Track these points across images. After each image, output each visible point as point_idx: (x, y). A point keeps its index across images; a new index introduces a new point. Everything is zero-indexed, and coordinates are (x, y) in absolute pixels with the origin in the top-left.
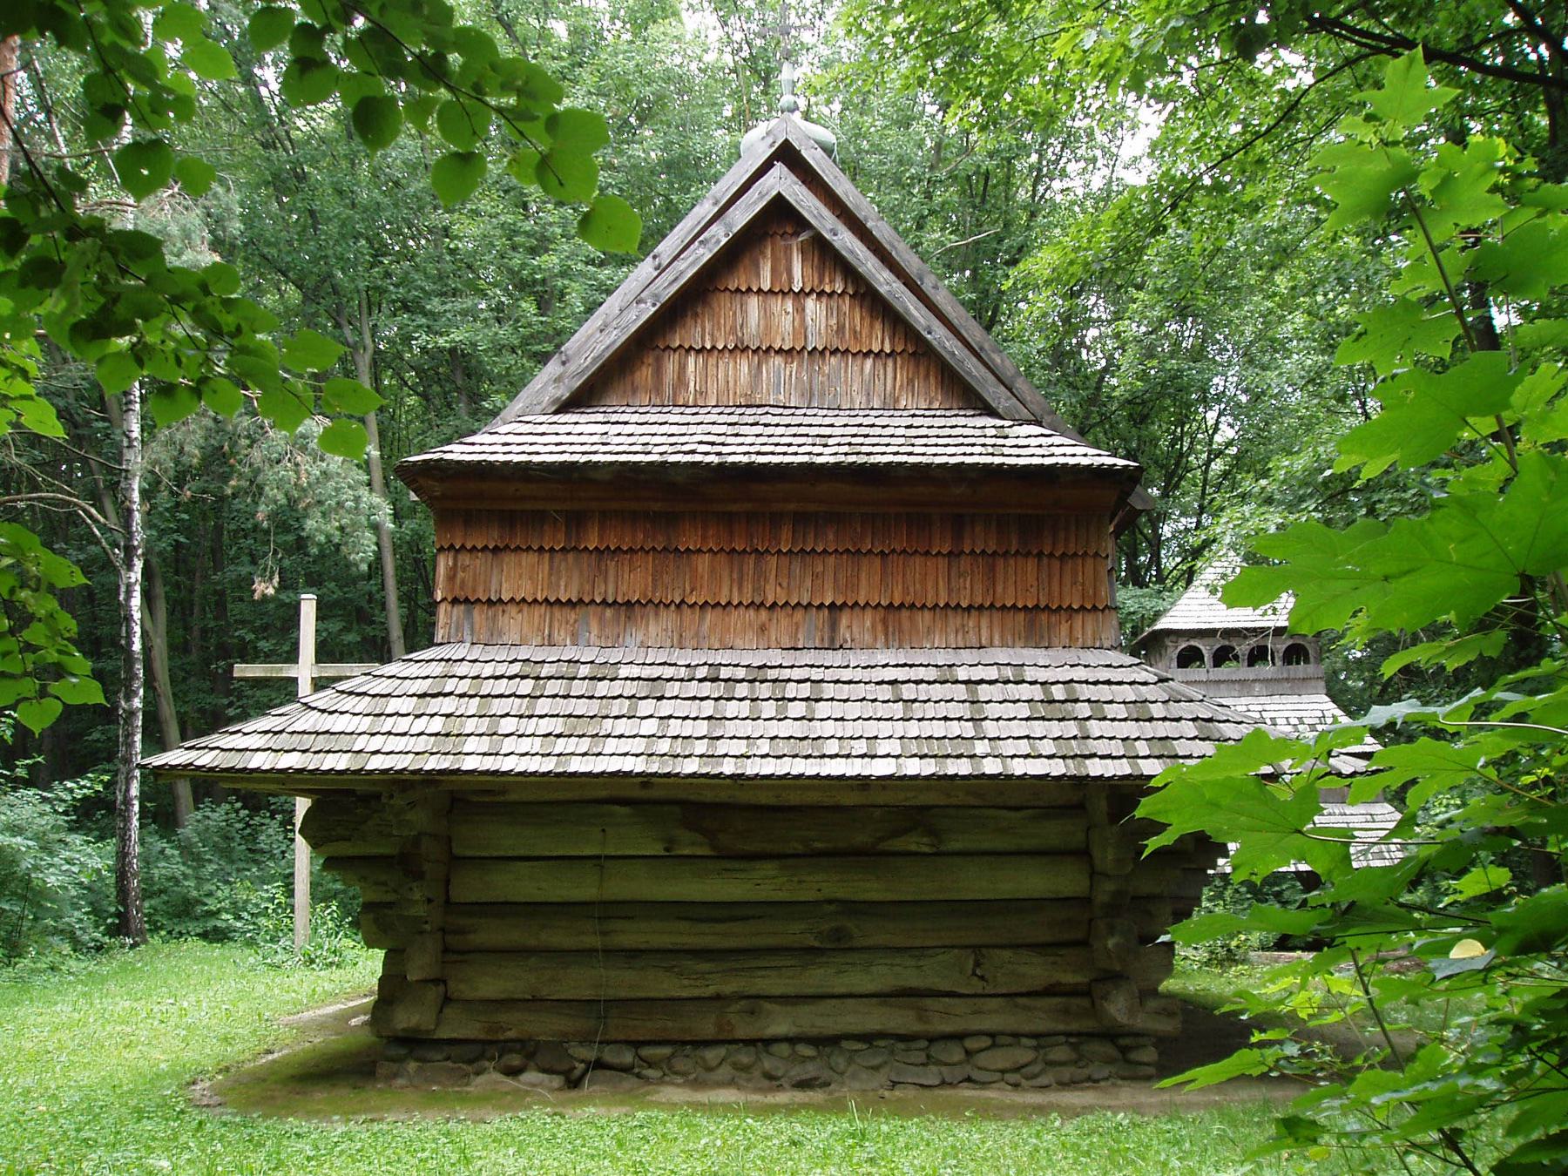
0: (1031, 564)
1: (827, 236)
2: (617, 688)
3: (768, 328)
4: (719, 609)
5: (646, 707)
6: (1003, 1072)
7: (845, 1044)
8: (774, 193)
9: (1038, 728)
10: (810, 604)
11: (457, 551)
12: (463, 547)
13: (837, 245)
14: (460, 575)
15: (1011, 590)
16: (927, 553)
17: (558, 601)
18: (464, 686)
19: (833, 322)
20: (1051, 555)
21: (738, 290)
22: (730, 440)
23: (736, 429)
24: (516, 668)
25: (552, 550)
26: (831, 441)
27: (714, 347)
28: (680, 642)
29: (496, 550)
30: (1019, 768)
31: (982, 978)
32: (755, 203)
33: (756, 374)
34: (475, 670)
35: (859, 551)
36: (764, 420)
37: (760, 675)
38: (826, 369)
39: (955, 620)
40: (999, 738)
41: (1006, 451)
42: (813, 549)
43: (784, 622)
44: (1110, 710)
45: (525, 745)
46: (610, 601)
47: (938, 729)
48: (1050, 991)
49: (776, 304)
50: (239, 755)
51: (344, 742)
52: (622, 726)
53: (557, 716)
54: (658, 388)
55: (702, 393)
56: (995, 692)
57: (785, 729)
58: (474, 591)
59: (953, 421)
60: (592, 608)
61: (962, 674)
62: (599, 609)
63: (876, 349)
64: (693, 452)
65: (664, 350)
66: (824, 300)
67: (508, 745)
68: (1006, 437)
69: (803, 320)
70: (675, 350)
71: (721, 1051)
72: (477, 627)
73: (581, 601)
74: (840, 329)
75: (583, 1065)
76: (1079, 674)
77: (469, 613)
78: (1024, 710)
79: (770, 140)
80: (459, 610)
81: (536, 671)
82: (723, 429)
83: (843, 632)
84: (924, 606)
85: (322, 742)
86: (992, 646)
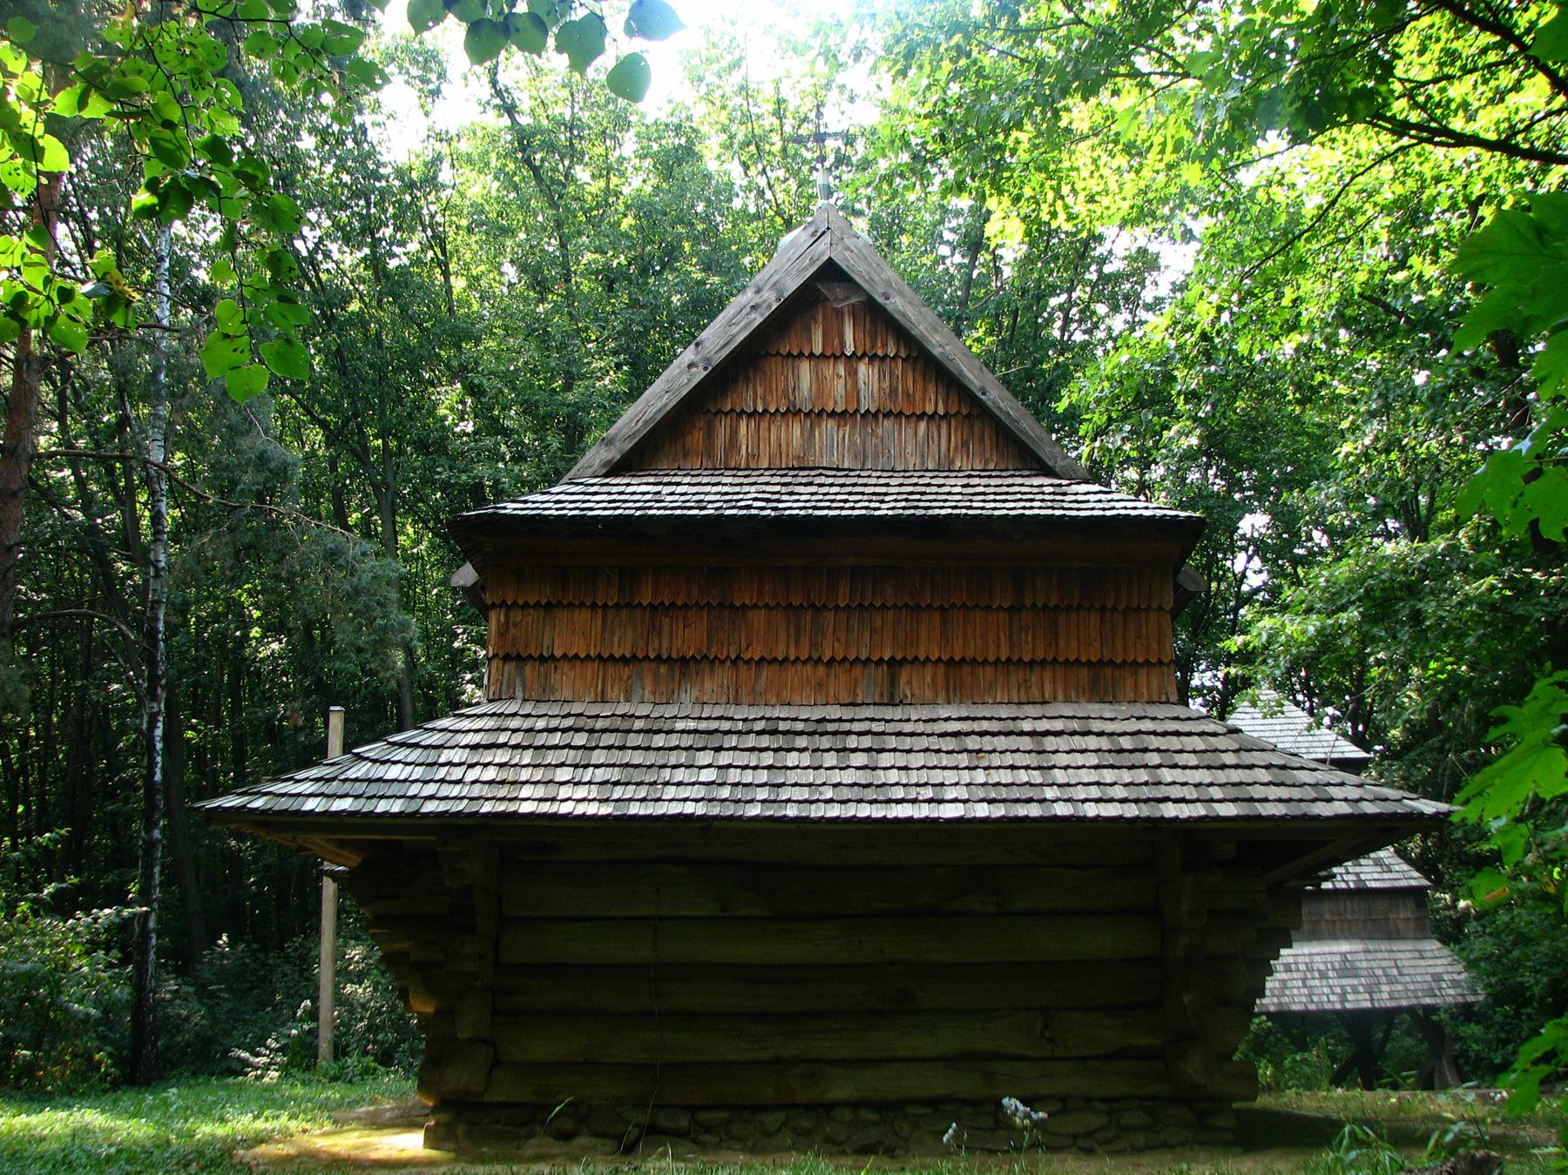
0: (1094, 618)
1: (880, 300)
2: (674, 740)
3: (820, 391)
4: (776, 666)
5: (704, 758)
6: (1075, 1136)
7: (910, 1110)
8: (825, 258)
9: (1108, 776)
10: (868, 659)
11: (509, 608)
12: (515, 603)
13: (889, 308)
14: (512, 631)
15: (1074, 644)
16: (988, 608)
17: (611, 656)
18: (517, 739)
19: (886, 385)
20: (1114, 609)
21: (790, 355)
22: (784, 498)
23: (790, 489)
24: (569, 722)
25: (605, 606)
26: (887, 498)
27: (765, 411)
28: (736, 697)
29: (549, 606)
30: (1091, 810)
31: (1051, 1040)
32: (806, 269)
34: (527, 724)
35: (918, 606)
36: (817, 480)
37: (821, 728)
38: (880, 431)
39: (1017, 676)
40: (1068, 785)
41: (1066, 505)
42: (871, 604)
43: (843, 678)
44: (1182, 759)
45: (581, 792)
47: (1005, 776)
48: (1120, 1054)
49: (828, 369)
50: (291, 800)
51: (395, 789)
52: (680, 775)
53: (613, 765)
54: (709, 451)
55: (756, 456)
56: (1062, 743)
57: (848, 777)
58: (526, 647)
59: (1010, 481)
60: (646, 665)
61: (1027, 726)
63: (930, 411)
64: (749, 507)
65: (715, 414)
66: (876, 364)
67: (565, 792)
68: (1065, 494)
69: (856, 383)
70: (726, 414)
71: (780, 1116)
72: (528, 683)
73: (634, 657)
74: (893, 392)
75: (637, 1131)
76: (1147, 725)
77: (520, 670)
78: (1093, 760)
79: (811, 230)
81: (590, 724)
82: (778, 488)
83: (903, 688)
84: (985, 661)
85: (373, 789)
86: (1055, 700)
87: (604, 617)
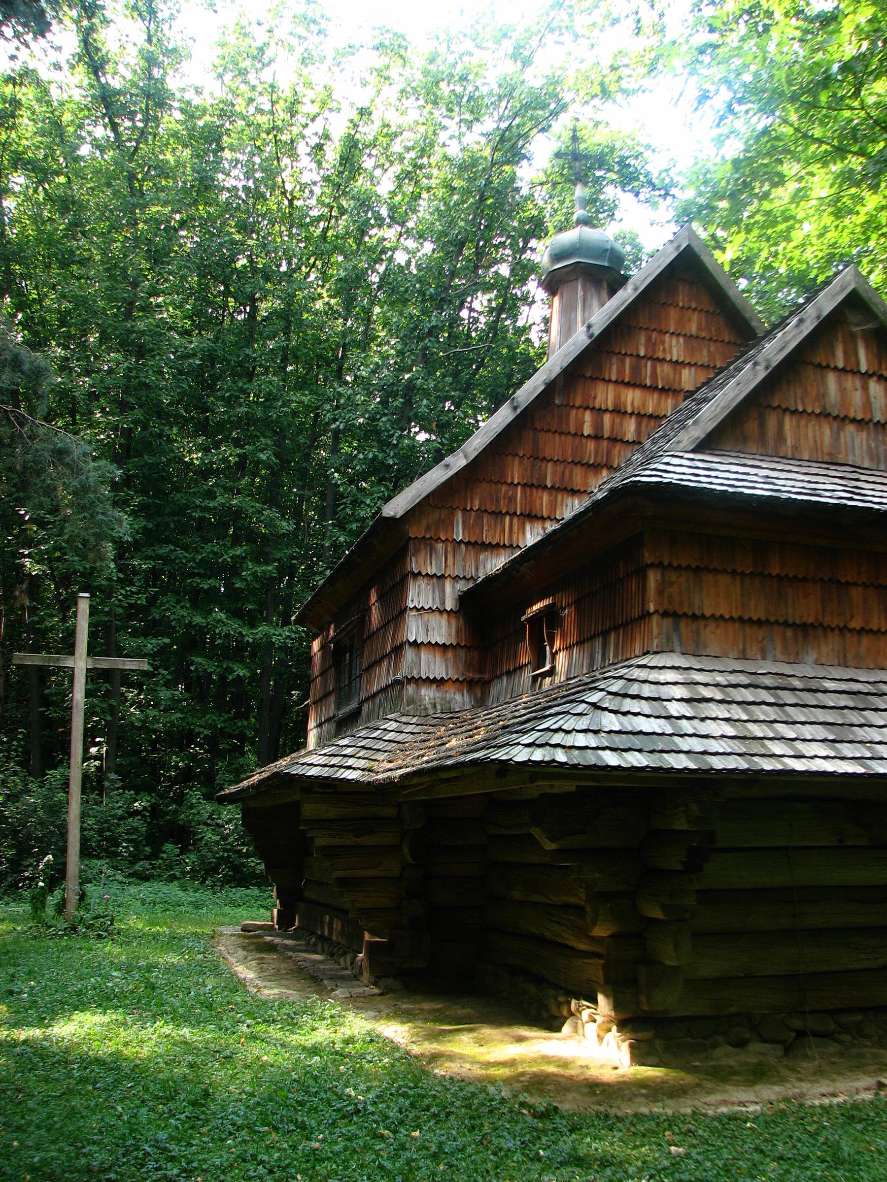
12: (670, 565)
17: (722, 617)
33: (836, 438)
46: (791, 621)
54: (762, 439)
58: (681, 605)
62: (781, 628)
70: (774, 409)
80: (668, 623)
87: (742, 583)
